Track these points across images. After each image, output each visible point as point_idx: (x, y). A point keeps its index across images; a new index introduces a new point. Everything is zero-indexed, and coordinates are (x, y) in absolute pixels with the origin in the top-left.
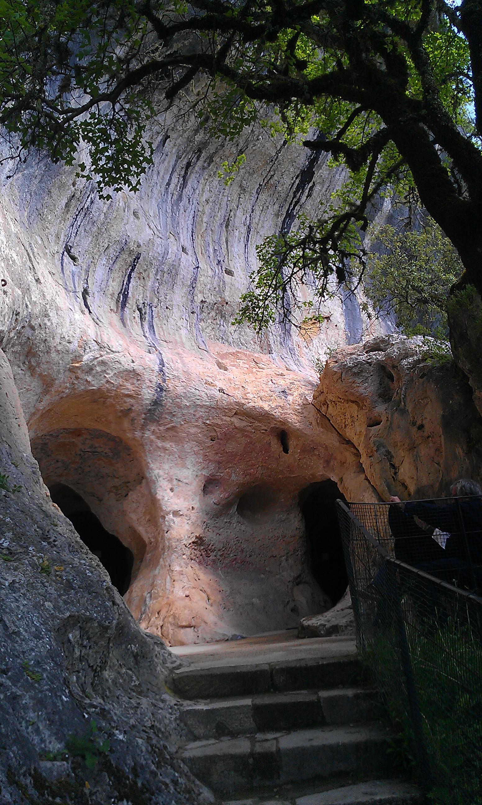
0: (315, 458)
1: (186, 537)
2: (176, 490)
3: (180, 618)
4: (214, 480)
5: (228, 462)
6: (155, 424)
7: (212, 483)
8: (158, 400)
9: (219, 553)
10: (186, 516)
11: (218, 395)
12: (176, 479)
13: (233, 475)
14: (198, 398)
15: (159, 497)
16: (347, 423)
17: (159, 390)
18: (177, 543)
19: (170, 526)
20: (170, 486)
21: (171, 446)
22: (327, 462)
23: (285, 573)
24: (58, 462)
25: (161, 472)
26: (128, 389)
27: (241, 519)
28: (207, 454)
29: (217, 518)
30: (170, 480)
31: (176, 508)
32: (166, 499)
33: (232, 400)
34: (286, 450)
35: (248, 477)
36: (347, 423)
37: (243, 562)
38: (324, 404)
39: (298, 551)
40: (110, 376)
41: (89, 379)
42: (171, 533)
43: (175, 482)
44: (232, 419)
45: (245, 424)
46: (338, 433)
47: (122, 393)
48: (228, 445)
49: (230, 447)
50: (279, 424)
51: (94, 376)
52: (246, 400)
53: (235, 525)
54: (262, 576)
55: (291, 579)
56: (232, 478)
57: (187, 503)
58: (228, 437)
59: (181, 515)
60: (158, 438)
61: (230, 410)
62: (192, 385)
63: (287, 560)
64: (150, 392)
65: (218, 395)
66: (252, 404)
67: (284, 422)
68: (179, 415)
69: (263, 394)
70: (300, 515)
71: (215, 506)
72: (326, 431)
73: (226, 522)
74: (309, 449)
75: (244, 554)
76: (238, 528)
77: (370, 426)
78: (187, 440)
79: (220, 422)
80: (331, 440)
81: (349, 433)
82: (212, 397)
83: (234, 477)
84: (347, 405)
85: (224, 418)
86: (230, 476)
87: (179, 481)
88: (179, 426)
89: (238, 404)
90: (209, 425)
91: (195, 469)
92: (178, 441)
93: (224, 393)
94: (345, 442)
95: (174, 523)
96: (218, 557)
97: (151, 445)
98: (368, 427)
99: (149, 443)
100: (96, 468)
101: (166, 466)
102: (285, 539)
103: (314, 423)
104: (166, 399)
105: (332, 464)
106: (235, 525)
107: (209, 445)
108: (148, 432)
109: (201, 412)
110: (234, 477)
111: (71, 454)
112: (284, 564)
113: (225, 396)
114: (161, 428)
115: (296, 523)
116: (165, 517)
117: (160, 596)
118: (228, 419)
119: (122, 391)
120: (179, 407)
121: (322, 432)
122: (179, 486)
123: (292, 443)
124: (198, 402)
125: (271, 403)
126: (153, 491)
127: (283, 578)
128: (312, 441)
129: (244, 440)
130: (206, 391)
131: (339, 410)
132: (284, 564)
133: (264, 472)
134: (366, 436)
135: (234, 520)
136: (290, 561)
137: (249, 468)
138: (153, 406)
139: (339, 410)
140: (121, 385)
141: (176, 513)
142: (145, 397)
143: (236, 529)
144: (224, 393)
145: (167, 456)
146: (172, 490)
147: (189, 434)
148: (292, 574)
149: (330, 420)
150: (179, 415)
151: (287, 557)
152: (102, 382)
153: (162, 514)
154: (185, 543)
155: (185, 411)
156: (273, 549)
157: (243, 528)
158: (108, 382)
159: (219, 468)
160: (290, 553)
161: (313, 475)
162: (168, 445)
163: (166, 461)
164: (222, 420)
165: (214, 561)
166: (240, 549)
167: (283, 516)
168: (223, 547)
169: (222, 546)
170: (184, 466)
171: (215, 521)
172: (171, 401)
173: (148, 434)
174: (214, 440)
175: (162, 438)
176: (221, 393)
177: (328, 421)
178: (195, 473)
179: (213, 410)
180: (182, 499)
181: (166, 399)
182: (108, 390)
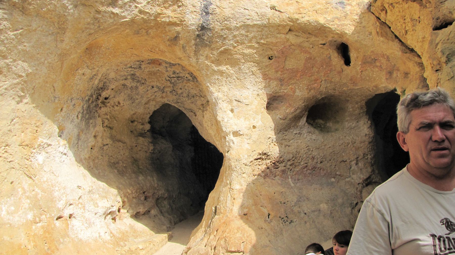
0: (377, 69)
1: (246, 156)
2: (235, 111)
3: (230, 243)
4: (279, 96)
5: (290, 79)
6: (207, 48)
7: (276, 100)
8: (204, 24)
9: (289, 163)
10: (247, 135)
11: (270, 13)
12: (236, 100)
13: (297, 91)
14: (248, 17)
15: (219, 119)
16: (407, 28)
17: (204, 14)
18: (236, 163)
19: (230, 147)
20: (230, 107)
21: (227, 68)
22: (390, 73)
23: (354, 176)
24: (153, 87)
25: (220, 95)
26: (169, 17)
27: (312, 129)
28: (267, 73)
29: (286, 131)
30: (230, 102)
31: (235, 128)
32: (226, 120)
33: (285, 16)
34: (347, 62)
35: (312, 91)
36: (407, 28)
37: (314, 168)
38: (382, 10)
39: (367, 155)
40: (143, 5)
41: (116, 10)
42: (231, 154)
43: (235, 103)
44: (288, 36)
45: (301, 40)
46: (400, 41)
47: (163, 22)
48: (287, 63)
49: (291, 64)
50: (336, 36)
51: (121, 7)
52: (300, 15)
53: (305, 135)
54: (333, 180)
55: (361, 181)
56: (297, 94)
57: (248, 123)
58: (285, 54)
59: (241, 135)
60: (213, 62)
61: (284, 26)
62: (241, 5)
63: (357, 164)
64: (194, 17)
65: (270, 13)
66: (307, 18)
67: (342, 35)
68: (230, 37)
69: (319, 6)
70: (369, 122)
71: (281, 121)
72: (387, 41)
73: (296, 134)
74: (370, 61)
75: (315, 161)
76: (308, 138)
77: (437, 28)
78: (243, 61)
79: (274, 40)
80: (394, 49)
81: (410, 41)
82: (263, 16)
83: (298, 93)
84: (406, 6)
85: (279, 35)
86: (294, 92)
87: (239, 101)
88: (232, 48)
89: (291, 20)
90: (264, 44)
91: (255, 88)
92: (234, 63)
93: (276, 10)
94: (408, 51)
95: (233, 143)
96: (288, 166)
97: (207, 69)
98: (434, 30)
99: (205, 68)
100: (186, 89)
101: (225, 89)
102: (355, 145)
103: (374, 32)
104: (214, 22)
105: (395, 75)
106: (305, 135)
107: (267, 64)
108: (201, 57)
109: (253, 31)
110: (298, 93)
111: (162, 80)
112: (354, 167)
113: (277, 13)
114: (215, 53)
115: (366, 129)
116: (225, 138)
117: (221, 213)
118: (283, 36)
119: (163, 20)
120: (229, 29)
121: (383, 42)
122: (239, 106)
123: (353, 55)
124: (249, 22)
125: (326, 16)
126: (215, 112)
127: (353, 181)
128: (372, 52)
129: (303, 56)
130: (256, 10)
131: (397, 14)
132: (354, 167)
133: (328, 85)
134: (431, 42)
135: (305, 131)
136: (360, 164)
137: (313, 82)
138: (201, 30)
139: (397, 14)
140: (160, 14)
141: (236, 134)
142: (190, 23)
143: (307, 139)
144: (276, 10)
145: (225, 79)
146: (232, 111)
147: (244, 55)
148: (362, 177)
149: (390, 28)
150: (230, 37)
151: (357, 161)
152: (134, 12)
153: (223, 135)
154: (245, 162)
155: (236, 33)
156: (343, 154)
157: (314, 137)
158: (141, 12)
159: (282, 85)
160: (360, 158)
161: (376, 86)
162: (223, 68)
163: (224, 83)
164: (277, 38)
165: (283, 172)
166: (311, 156)
167: (353, 124)
168: (293, 157)
169: (292, 156)
170: (244, 87)
171: (283, 134)
172: (219, 23)
173: (202, 59)
174: (271, 59)
175: (218, 62)
176: (273, 11)
177: (388, 29)
178: (256, 93)
179: (266, 29)
180: (242, 119)
181: (214, 22)
182: (145, 21)
